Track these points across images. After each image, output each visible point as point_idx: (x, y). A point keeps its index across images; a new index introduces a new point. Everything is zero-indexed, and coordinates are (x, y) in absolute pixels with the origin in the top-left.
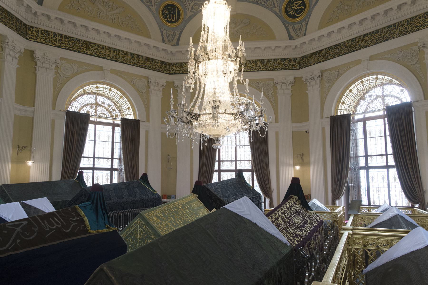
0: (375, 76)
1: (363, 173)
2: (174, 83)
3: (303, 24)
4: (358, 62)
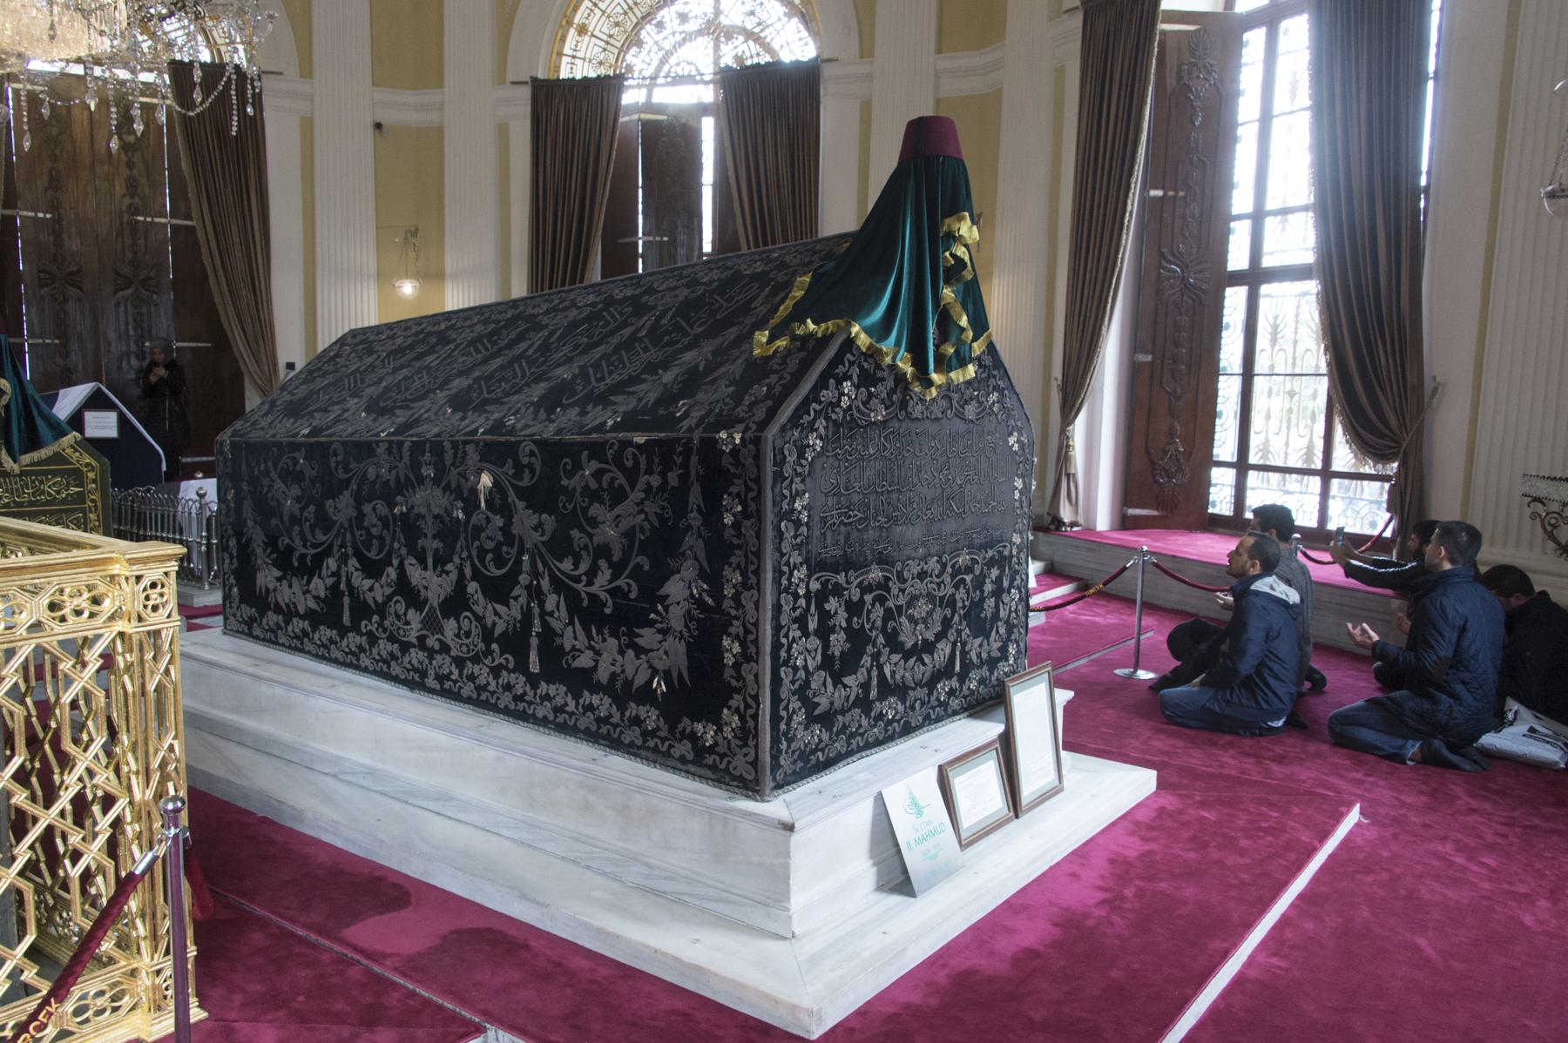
1: (1235, 300)
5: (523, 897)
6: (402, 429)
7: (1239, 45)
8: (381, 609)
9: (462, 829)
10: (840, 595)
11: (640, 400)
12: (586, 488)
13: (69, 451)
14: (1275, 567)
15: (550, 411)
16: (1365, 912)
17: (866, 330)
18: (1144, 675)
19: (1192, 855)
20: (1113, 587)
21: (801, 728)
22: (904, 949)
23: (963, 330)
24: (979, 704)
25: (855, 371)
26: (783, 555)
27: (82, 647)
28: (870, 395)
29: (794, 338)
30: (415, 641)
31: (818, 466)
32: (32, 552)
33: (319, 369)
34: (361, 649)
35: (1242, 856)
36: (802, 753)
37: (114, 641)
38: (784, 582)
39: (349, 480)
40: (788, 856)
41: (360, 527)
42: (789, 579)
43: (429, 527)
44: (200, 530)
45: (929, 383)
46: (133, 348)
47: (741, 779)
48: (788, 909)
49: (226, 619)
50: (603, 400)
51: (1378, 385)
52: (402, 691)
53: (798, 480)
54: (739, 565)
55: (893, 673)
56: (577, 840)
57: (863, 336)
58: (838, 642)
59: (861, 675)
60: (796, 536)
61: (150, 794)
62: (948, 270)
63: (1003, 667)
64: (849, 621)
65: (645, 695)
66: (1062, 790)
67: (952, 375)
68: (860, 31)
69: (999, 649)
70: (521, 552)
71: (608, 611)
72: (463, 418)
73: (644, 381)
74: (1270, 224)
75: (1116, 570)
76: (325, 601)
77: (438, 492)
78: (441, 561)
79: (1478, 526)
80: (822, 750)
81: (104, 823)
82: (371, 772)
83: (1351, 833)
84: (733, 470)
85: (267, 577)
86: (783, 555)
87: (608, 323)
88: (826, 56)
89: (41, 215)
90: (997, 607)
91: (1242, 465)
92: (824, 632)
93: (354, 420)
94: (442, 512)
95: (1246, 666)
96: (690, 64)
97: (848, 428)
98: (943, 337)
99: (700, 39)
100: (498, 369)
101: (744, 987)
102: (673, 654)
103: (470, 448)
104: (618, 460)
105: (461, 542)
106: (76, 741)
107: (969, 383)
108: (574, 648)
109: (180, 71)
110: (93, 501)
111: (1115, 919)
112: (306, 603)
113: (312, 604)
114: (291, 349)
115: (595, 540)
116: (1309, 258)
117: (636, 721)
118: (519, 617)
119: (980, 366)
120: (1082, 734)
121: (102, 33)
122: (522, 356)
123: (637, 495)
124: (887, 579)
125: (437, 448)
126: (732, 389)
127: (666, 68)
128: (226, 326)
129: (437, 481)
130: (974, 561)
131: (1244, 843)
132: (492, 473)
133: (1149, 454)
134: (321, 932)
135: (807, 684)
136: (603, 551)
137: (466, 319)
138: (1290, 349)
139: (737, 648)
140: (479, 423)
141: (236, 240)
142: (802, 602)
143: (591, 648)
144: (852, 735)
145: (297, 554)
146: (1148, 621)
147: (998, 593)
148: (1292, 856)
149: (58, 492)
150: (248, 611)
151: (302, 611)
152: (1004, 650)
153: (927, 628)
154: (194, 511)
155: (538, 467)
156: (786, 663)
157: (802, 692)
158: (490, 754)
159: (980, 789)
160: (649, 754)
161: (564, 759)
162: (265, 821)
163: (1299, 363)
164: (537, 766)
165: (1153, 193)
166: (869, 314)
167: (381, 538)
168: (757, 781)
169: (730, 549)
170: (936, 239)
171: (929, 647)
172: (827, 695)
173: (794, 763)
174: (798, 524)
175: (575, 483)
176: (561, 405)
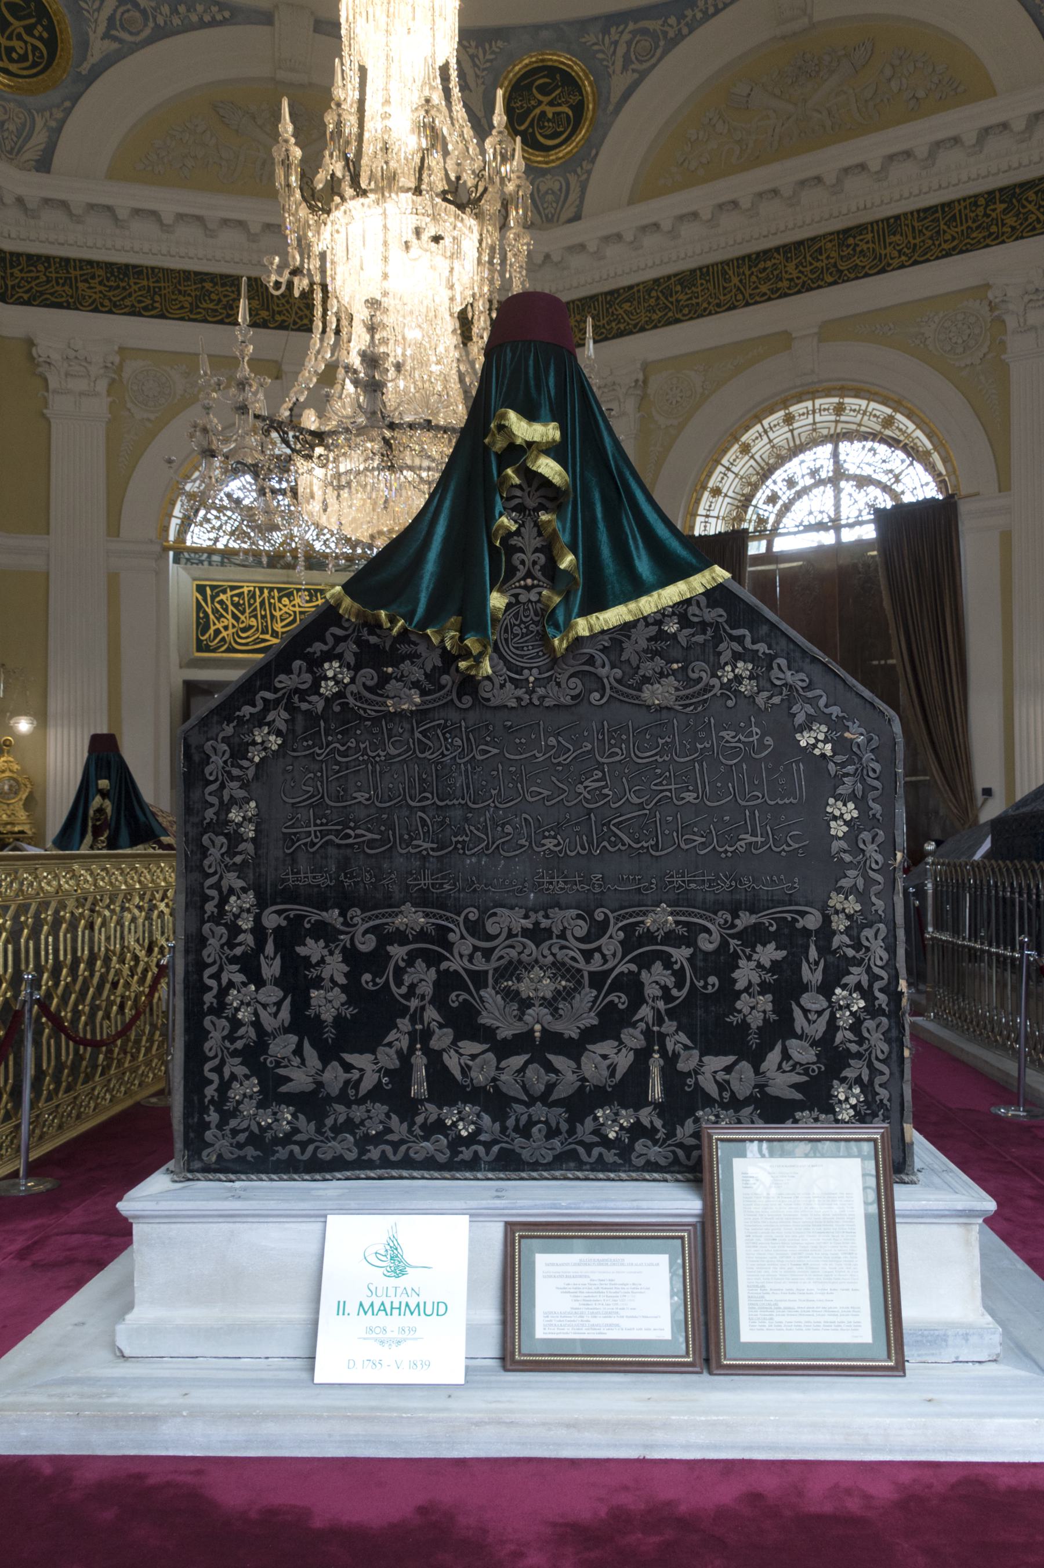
0: (836, 400)
2: (30, 343)
3: (573, 179)
4: (783, 340)
57: (347, 602)
157: (253, 1056)
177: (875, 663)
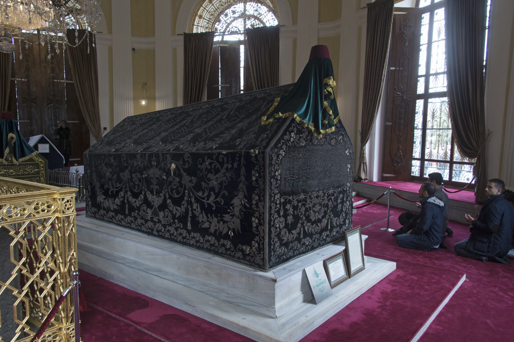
1: (420, 104)
5: (187, 304)
6: (145, 149)
7: (421, 18)
8: (139, 209)
9: (166, 282)
10: (291, 204)
11: (224, 139)
12: (207, 168)
13: (35, 157)
14: (434, 193)
15: (194, 143)
16: (469, 311)
17: (299, 116)
18: (390, 230)
19: (409, 291)
20: (380, 200)
21: (278, 247)
22: (313, 322)
23: (330, 115)
24: (336, 240)
25: (295, 129)
26: (272, 190)
27: (44, 222)
28: (300, 137)
29: (275, 119)
30: (150, 219)
31: (283, 161)
32: (27, 191)
33: (117, 130)
34: (132, 222)
35: (426, 291)
36: (278, 256)
37: (55, 220)
38: (273, 199)
39: (128, 166)
40: (274, 290)
41: (131, 182)
42: (274, 198)
43: (154, 181)
44: (76, 183)
45: (320, 133)
46: (53, 123)
47: (258, 264)
48: (275, 308)
49: (87, 212)
50: (212, 139)
51: (469, 132)
52: (145, 235)
53: (277, 165)
54: (257, 194)
55: (308, 230)
56: (204, 285)
57: (298, 118)
58: (290, 219)
59: (298, 230)
60: (276, 184)
61: (66, 270)
62: (325, 96)
63: (344, 228)
64: (293, 212)
65: (226, 237)
66: (364, 269)
67: (327, 130)
68: (293, 16)
69: (343, 221)
70: (185, 190)
71: (214, 209)
72: (166, 146)
73: (225, 133)
74: (431, 78)
75: (380, 195)
76: (120, 206)
77: (157, 170)
78: (158, 193)
79: (504, 180)
80: (285, 255)
81: (51, 280)
82: (135, 262)
83: (463, 284)
84: (255, 162)
85: (100, 198)
86: (272, 190)
87: (213, 114)
88: (281, 24)
89: (23, 80)
90: (342, 207)
91: (422, 159)
92: (285, 216)
93: (129, 146)
94: (159, 177)
95: (426, 228)
96: (236, 27)
97: (293, 148)
98: (324, 118)
99: (239, 19)
100: (177, 129)
101: (260, 334)
102: (236, 223)
103: (168, 155)
104: (217, 159)
105: (165, 186)
106: (42, 252)
107: (332, 133)
108: (202, 221)
109: (70, 33)
110: (42, 174)
111: (384, 312)
112: (113, 207)
113: (115, 207)
114: (105, 123)
115: (210, 185)
116: (445, 90)
117: (223, 245)
118: (184, 211)
119: (336, 127)
120: (370, 250)
121: (46, 21)
122: (184, 125)
123: (223, 171)
124: (306, 198)
125: (157, 155)
126: (255, 135)
127: (228, 29)
128: (84, 116)
129: (157, 166)
130: (335, 192)
131: (427, 287)
132: (175, 164)
133: (391, 155)
134: (120, 315)
135: (280, 233)
136: (212, 189)
137: (165, 113)
138: (438, 120)
139: (257, 221)
140: (171, 148)
141: (87, 87)
142: (278, 206)
143: (208, 221)
144: (295, 250)
145: (110, 191)
146: (392, 212)
147: (342, 202)
148: (443, 292)
149: (31, 171)
150: (94, 209)
151: (112, 209)
152: (344, 221)
153: (319, 214)
154: (75, 177)
155: (190, 162)
156: (273, 226)
157: (278, 236)
158: (175, 256)
159: (337, 268)
160: (228, 256)
161: (201, 258)
162: (100, 279)
163: (442, 125)
164: (190, 260)
165: (392, 68)
166: (299, 111)
167: (138, 185)
168: (264, 265)
169: (255, 188)
170: (322, 85)
171: (320, 221)
172: (287, 237)
173: (276, 259)
174: (277, 180)
175: (203, 167)
176: (198, 141)
177: (56, 80)
